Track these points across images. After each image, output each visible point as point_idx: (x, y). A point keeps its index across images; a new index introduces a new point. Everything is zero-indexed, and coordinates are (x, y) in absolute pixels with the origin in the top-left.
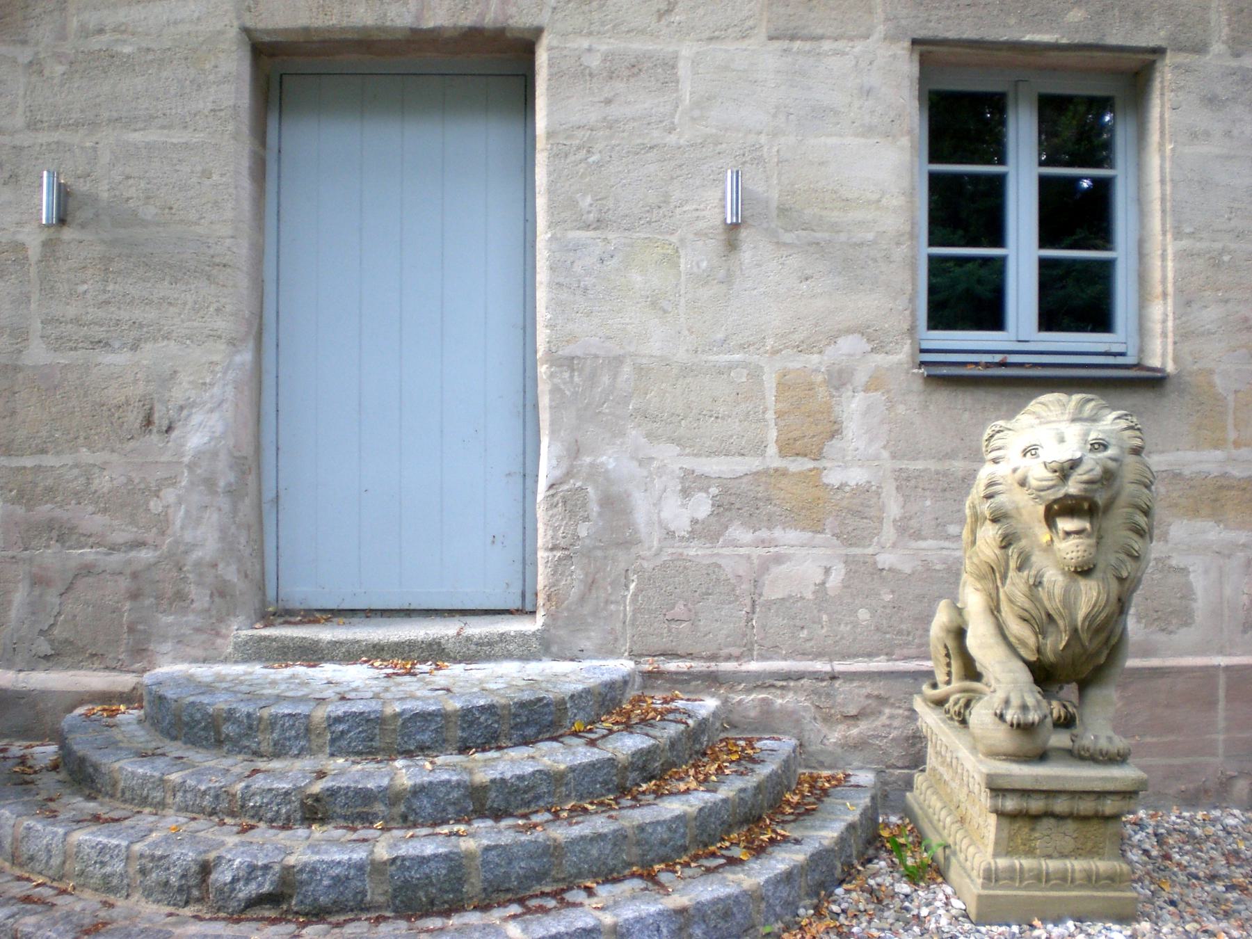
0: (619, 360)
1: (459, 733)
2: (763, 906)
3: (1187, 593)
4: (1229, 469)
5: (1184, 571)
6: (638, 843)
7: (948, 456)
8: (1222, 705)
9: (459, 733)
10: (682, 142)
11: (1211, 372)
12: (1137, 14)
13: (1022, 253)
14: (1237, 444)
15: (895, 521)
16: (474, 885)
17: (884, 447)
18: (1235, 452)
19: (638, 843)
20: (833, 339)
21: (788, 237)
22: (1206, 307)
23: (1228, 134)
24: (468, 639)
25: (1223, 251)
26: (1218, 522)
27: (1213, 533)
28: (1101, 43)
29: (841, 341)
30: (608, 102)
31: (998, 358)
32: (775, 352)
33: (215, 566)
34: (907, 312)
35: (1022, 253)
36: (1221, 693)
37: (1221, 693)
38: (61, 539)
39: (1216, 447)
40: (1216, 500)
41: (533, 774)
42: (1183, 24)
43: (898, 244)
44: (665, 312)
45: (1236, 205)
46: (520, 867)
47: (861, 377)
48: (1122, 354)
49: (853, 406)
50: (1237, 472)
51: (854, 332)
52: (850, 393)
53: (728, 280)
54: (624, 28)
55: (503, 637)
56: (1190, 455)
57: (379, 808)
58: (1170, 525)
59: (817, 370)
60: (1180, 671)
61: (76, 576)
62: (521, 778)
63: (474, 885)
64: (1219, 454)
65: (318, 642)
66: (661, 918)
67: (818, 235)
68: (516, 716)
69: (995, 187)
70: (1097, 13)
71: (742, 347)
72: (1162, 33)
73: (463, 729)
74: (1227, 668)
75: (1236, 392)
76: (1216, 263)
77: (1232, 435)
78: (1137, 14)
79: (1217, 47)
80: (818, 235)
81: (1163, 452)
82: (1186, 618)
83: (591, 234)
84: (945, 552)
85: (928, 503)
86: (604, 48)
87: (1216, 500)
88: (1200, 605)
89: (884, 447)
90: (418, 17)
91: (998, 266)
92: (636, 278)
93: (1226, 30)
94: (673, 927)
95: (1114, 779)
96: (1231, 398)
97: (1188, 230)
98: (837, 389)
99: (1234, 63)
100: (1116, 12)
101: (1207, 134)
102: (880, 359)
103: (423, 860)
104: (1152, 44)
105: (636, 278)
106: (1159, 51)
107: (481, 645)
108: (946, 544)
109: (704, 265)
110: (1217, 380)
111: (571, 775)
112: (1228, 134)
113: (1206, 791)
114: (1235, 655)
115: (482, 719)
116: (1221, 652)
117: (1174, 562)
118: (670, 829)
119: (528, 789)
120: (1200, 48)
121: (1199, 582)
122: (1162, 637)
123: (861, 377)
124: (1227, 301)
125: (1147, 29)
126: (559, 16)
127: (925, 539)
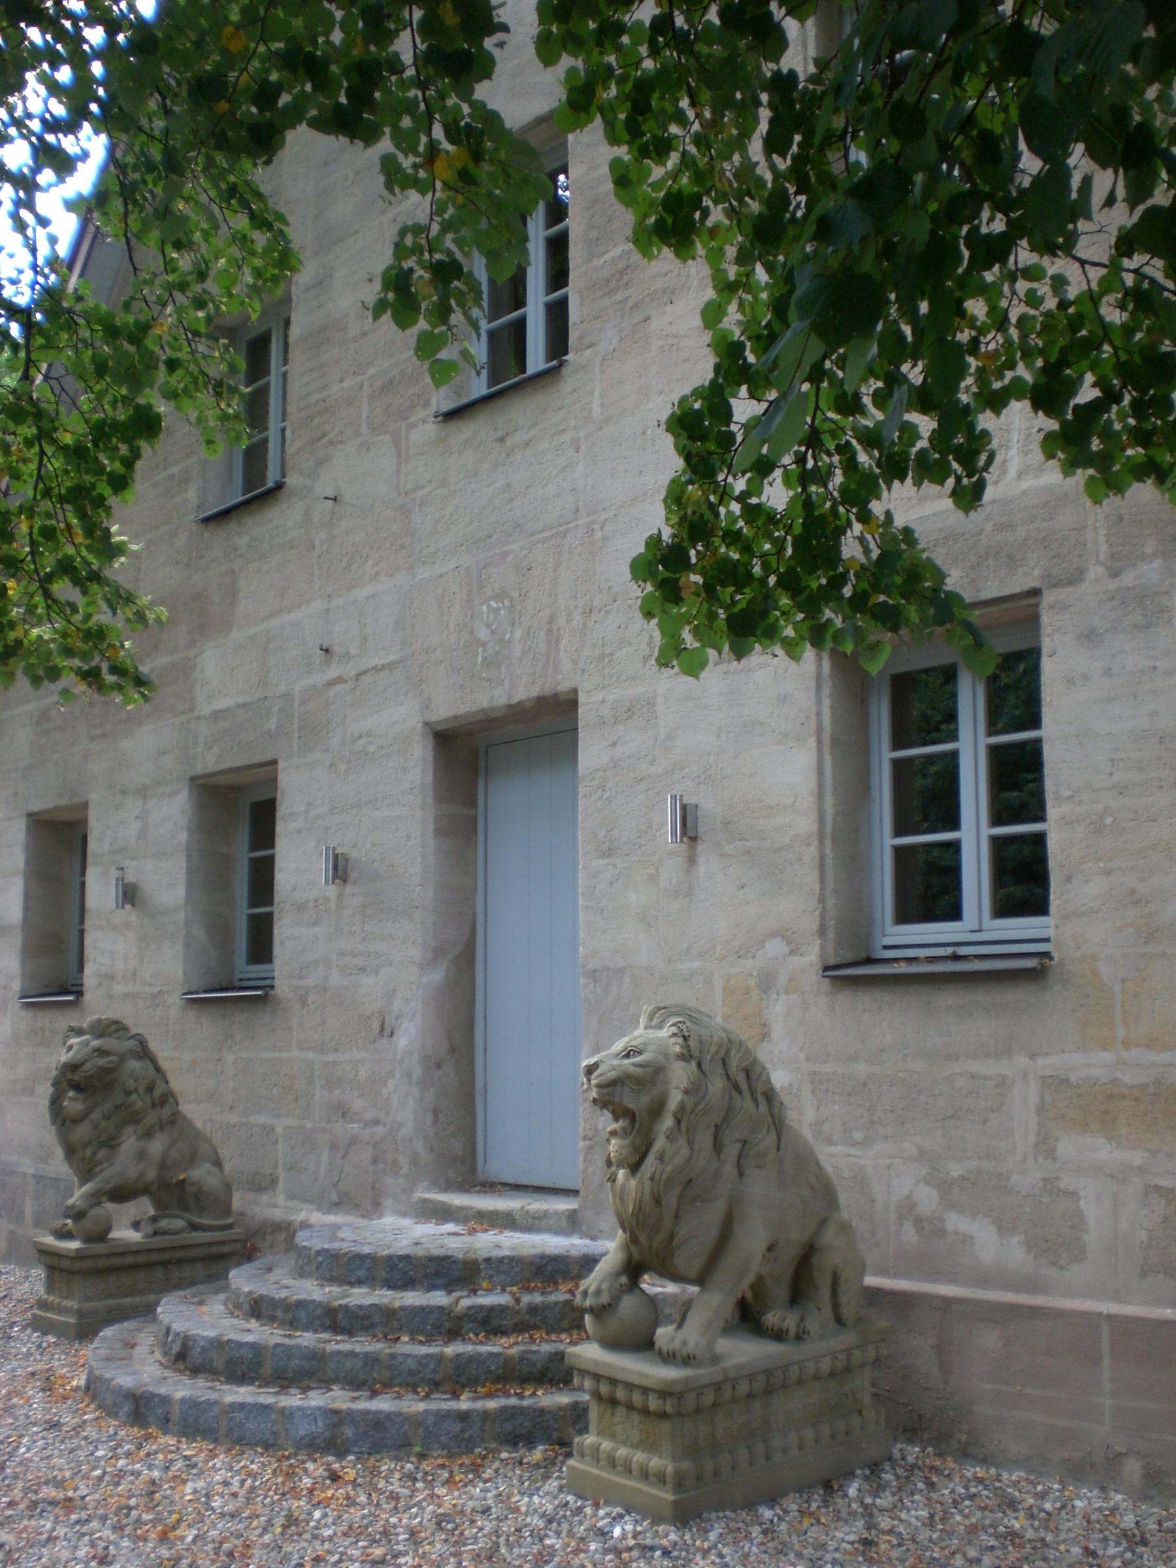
0: (622, 971)
1: (384, 1275)
2: (421, 1430)
3: (1078, 1222)
4: (1119, 1075)
5: (1073, 1195)
6: (388, 1367)
7: (853, 1059)
8: (1106, 1361)
9: (384, 1275)
10: (660, 771)
11: (1095, 958)
12: (1010, 557)
13: (975, 835)
14: (1127, 1044)
15: (811, 1125)
16: (267, 1369)
17: (801, 1050)
18: (1124, 1054)
19: (388, 1367)
20: (762, 944)
21: (729, 849)
22: (1087, 882)
23: (1108, 672)
24: (527, 1212)
25: (1107, 811)
26: (1109, 1139)
27: (1104, 1152)
28: (977, 600)
29: (767, 944)
30: (614, 744)
31: (949, 951)
32: (723, 958)
33: (411, 1141)
34: (817, 913)
35: (975, 835)
36: (1105, 1347)
37: (1105, 1347)
38: (343, 1115)
39: (1104, 1048)
40: (1107, 1112)
41: (370, 1306)
42: (1057, 556)
43: (808, 845)
44: (650, 926)
45: (1118, 756)
46: (296, 1363)
47: (782, 980)
48: (1047, 940)
49: (777, 1008)
50: (1128, 1078)
51: (776, 936)
52: (775, 996)
53: (689, 894)
54: (623, 678)
55: (546, 1214)
56: (1077, 1058)
57: (279, 1313)
58: (1057, 1140)
59: (750, 975)
60: (1060, 1314)
61: (349, 1144)
62: (360, 1307)
63: (267, 1369)
64: (1108, 1057)
65: (450, 1206)
66: (318, 1413)
67: (749, 844)
68: (426, 1267)
69: (949, 766)
70: (972, 567)
71: (701, 955)
72: (1036, 572)
73: (387, 1273)
74: (1109, 1317)
75: (1123, 981)
76: (1098, 829)
77: (1121, 1032)
78: (1010, 557)
79: (1095, 572)
80: (749, 844)
81: (1047, 1054)
82: (1078, 1253)
83: (606, 861)
84: (852, 1159)
85: (837, 1107)
86: (611, 698)
87: (1107, 1112)
88: (1092, 1238)
89: (801, 1050)
90: (510, 697)
91: (954, 847)
92: (633, 897)
93: (1104, 548)
94: (327, 1421)
95: (647, 1376)
96: (1118, 987)
97: (1067, 793)
98: (764, 992)
99: (1112, 585)
100: (991, 561)
101: (1085, 677)
102: (796, 960)
103: (241, 1345)
104: (1026, 588)
105: (633, 897)
106: (1035, 593)
107: (533, 1218)
108: (852, 1151)
109: (674, 880)
110: (1103, 968)
111: (402, 1313)
112: (1108, 672)
113: (1092, 1466)
114: (1131, 1303)
115: (401, 1265)
116: (1117, 1298)
117: (1063, 1184)
118: (420, 1363)
119: (367, 1317)
120: (1074, 579)
121: (1091, 1211)
122: (1051, 1272)
123: (782, 980)
124: (1109, 873)
125: (1020, 571)
126: (586, 676)
127: (835, 1144)
